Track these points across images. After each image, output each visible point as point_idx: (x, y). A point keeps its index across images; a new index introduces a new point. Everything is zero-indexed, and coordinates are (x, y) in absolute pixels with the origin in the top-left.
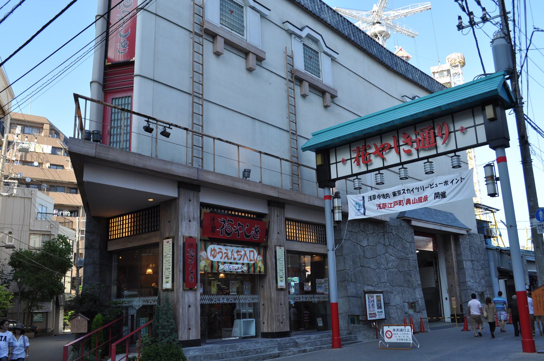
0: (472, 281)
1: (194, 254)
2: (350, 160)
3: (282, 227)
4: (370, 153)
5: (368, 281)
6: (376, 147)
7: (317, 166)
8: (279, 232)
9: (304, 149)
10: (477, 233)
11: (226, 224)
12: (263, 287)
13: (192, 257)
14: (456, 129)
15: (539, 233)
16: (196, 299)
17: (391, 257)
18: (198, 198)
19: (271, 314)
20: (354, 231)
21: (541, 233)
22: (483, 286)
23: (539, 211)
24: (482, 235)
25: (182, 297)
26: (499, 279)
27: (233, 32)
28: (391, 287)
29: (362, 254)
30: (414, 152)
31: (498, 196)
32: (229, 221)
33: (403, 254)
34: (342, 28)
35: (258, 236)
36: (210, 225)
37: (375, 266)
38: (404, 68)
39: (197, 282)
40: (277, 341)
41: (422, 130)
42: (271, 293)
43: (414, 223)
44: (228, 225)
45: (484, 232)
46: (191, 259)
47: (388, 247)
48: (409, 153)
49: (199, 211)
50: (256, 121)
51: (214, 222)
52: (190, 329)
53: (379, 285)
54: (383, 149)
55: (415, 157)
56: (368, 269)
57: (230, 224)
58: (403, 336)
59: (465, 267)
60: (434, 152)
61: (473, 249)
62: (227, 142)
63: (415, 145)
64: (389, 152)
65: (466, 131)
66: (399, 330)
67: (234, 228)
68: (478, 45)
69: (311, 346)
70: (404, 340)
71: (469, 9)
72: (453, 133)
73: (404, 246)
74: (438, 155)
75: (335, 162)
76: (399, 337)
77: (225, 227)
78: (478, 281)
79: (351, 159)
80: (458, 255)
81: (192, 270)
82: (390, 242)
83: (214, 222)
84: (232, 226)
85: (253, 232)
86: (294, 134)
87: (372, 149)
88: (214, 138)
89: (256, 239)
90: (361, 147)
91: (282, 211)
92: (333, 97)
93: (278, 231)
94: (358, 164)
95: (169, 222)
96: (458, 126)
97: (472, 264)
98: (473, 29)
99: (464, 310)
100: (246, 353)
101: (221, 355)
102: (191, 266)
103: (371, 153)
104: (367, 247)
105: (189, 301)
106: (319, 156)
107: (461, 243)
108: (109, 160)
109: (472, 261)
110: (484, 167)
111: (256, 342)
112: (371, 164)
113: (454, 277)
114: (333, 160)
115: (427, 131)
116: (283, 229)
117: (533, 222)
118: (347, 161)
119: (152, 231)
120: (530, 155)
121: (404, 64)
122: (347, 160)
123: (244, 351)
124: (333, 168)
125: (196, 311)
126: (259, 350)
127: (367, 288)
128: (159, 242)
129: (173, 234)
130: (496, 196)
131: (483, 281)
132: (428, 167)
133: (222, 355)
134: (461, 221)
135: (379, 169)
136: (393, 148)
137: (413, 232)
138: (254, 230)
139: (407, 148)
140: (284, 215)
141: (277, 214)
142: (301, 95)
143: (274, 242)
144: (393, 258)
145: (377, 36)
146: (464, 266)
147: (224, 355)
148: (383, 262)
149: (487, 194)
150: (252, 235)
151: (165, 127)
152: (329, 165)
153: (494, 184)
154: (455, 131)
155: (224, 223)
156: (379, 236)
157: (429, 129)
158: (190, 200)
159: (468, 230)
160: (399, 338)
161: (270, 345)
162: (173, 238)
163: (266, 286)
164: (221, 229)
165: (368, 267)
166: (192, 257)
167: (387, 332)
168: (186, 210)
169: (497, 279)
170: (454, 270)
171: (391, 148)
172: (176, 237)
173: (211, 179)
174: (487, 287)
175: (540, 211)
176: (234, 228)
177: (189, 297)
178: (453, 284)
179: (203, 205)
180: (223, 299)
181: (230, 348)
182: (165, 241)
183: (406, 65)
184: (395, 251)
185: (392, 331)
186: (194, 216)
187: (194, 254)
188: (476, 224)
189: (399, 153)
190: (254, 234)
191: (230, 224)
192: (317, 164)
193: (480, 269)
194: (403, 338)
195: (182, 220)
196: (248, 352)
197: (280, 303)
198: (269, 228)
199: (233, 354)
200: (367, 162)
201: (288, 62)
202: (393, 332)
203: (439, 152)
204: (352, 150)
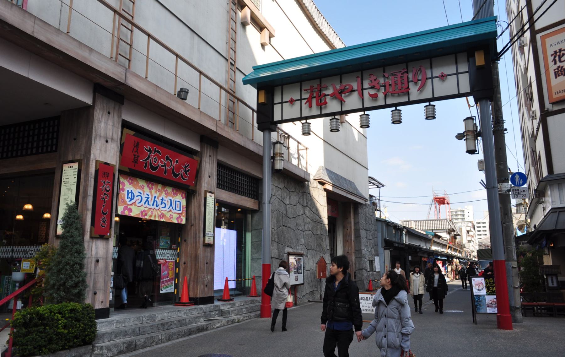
0: (365, 250)
3: (214, 170)
4: (327, 94)
5: (288, 242)
6: (335, 88)
7: (258, 104)
8: (210, 175)
11: (152, 155)
12: (185, 241)
13: (106, 192)
14: (434, 76)
17: (308, 219)
19: (195, 275)
20: (279, 187)
22: (372, 255)
25: (88, 246)
26: (385, 249)
28: (306, 250)
29: (284, 212)
30: (381, 95)
31: (478, 153)
35: (187, 177)
36: (132, 152)
37: (294, 226)
39: (111, 227)
40: (201, 309)
41: (393, 74)
42: (196, 249)
44: (154, 156)
46: (105, 194)
47: (306, 208)
48: (374, 97)
50: (195, 35)
51: (137, 149)
52: (95, 294)
53: (297, 248)
54: (342, 92)
55: (381, 102)
57: (156, 155)
59: (361, 236)
60: (405, 99)
63: (383, 90)
64: (348, 96)
65: (446, 79)
66: (364, 298)
69: (237, 315)
70: (369, 310)
72: (431, 80)
75: (280, 101)
77: (150, 159)
78: (369, 250)
79: (301, 100)
80: (356, 224)
81: (105, 209)
82: (308, 203)
83: (137, 149)
85: (182, 171)
87: (330, 90)
89: (185, 180)
90: (316, 86)
91: (215, 151)
92: (271, 36)
93: (209, 174)
94: (310, 106)
96: (437, 72)
97: (366, 233)
99: (357, 277)
100: (168, 327)
101: (137, 330)
102: (104, 204)
103: (328, 95)
104: (289, 206)
105: (97, 253)
107: (359, 212)
109: (366, 230)
110: (464, 120)
111: (178, 311)
112: (326, 107)
113: (351, 244)
114: (277, 99)
115: (399, 75)
116: (214, 172)
117: (502, 187)
118: (296, 102)
119: (42, 152)
123: (167, 323)
124: (277, 109)
126: (184, 322)
128: (55, 168)
129: (81, 157)
130: (476, 153)
131: (373, 249)
132: (396, 116)
133: (139, 330)
135: (333, 114)
136: (355, 91)
138: (183, 169)
139: (372, 92)
140: (216, 157)
141: (210, 153)
142: (241, 23)
143: (204, 187)
144: (309, 220)
146: (360, 235)
147: (141, 330)
148: (301, 223)
149: (466, 150)
150: (180, 174)
152: (273, 104)
154: (432, 78)
155: (150, 153)
156: (299, 196)
157: (402, 73)
158: (109, 113)
161: (195, 313)
162: (80, 162)
163: (190, 240)
164: (145, 160)
165: (289, 227)
166: (106, 192)
168: (103, 125)
170: (351, 238)
171: (352, 91)
172: (84, 162)
175: (517, 174)
177: (97, 248)
178: (350, 252)
179: (125, 125)
182: (66, 167)
186: (112, 135)
189: (362, 95)
192: (259, 102)
193: (371, 238)
194: (368, 309)
195: (95, 138)
196: (172, 325)
197: (206, 262)
198: (199, 169)
199: (153, 329)
200: (321, 104)
203: (411, 100)
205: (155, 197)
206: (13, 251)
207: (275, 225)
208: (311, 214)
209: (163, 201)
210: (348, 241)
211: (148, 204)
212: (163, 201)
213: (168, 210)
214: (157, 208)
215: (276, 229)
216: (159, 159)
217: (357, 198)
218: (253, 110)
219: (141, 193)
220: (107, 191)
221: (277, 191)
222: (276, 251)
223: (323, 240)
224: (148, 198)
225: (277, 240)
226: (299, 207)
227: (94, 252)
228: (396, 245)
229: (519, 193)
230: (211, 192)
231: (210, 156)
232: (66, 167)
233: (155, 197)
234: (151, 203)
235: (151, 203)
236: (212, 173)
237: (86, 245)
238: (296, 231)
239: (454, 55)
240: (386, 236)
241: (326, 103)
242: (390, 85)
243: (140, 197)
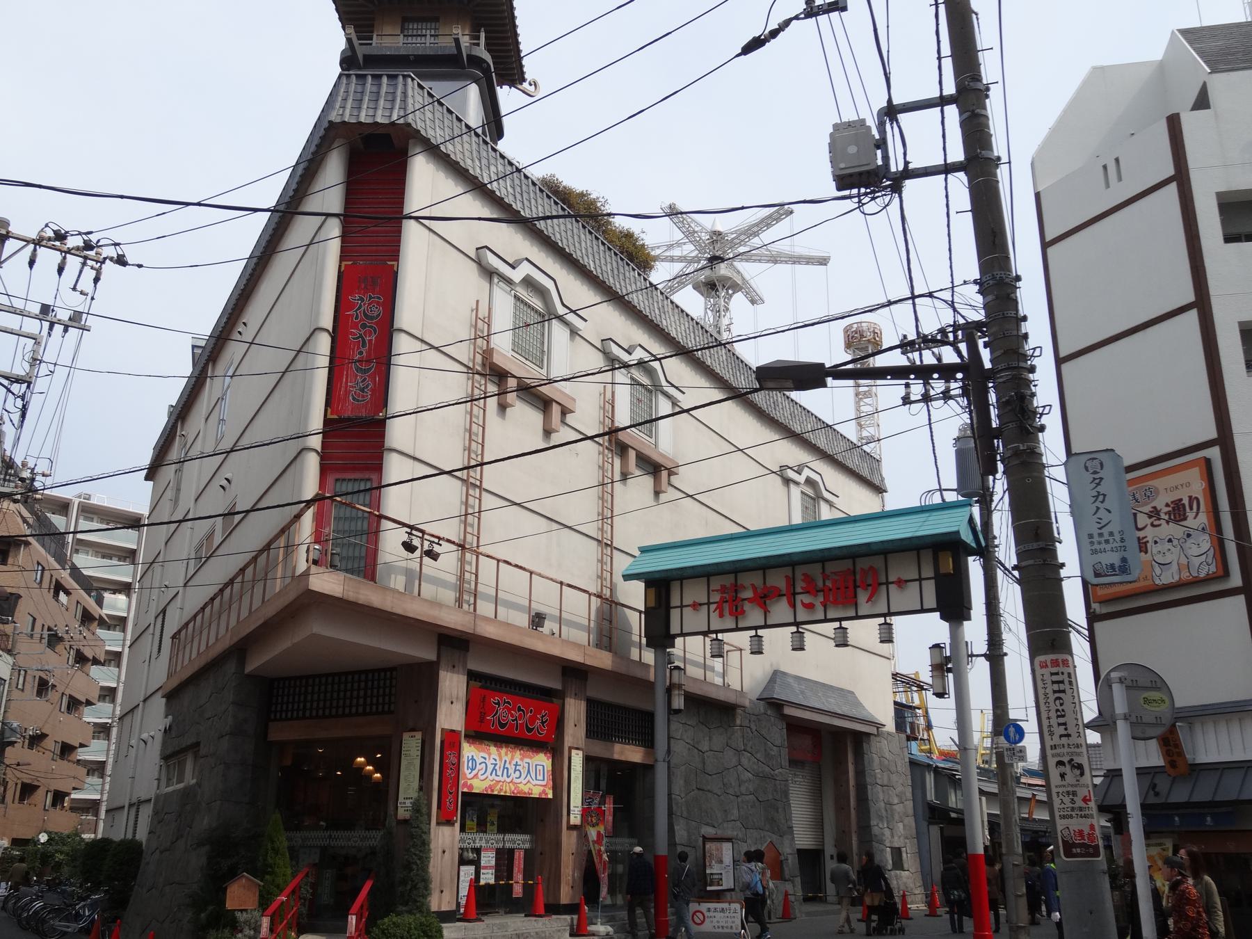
1: (455, 761)
2: (706, 606)
9: (627, 577)
10: (894, 731)
12: (542, 821)
15: (1007, 761)
16: (453, 840)
18: (465, 664)
21: (1010, 762)
22: (900, 837)
23: (1009, 726)
24: (903, 736)
26: (930, 823)
27: (527, 362)
32: (505, 702)
33: (767, 769)
34: (693, 342)
35: (544, 730)
38: (789, 412)
43: (788, 711)
45: (906, 728)
47: (743, 755)
49: (465, 685)
52: (442, 892)
56: (710, 795)
57: (506, 707)
58: (724, 920)
61: (886, 762)
62: (516, 566)
67: (512, 716)
68: (940, 474)
71: (923, 358)
73: (769, 754)
74: (857, 617)
76: (718, 922)
81: (451, 788)
84: (509, 710)
86: (606, 545)
88: (498, 561)
94: (721, 616)
95: (416, 702)
98: (928, 406)
103: (745, 599)
106: (652, 591)
107: (865, 752)
108: (360, 602)
114: (675, 601)
120: (1002, 633)
121: (789, 404)
122: (701, 605)
124: (675, 615)
125: (453, 859)
127: (708, 831)
134: (866, 707)
136: (784, 595)
137: (785, 726)
139: (807, 599)
145: (716, 286)
151: (432, 542)
152: (668, 608)
153: (943, 677)
154: (887, 583)
158: (454, 667)
159: (879, 726)
160: (716, 925)
165: (709, 791)
167: (695, 913)
168: (447, 683)
169: (925, 824)
173: (490, 631)
174: (906, 838)
176: (512, 716)
177: (443, 835)
180: (481, 839)
181: (499, 929)
182: (406, 736)
183: (791, 404)
184: (754, 763)
185: (704, 911)
187: (455, 761)
188: (893, 714)
189: (793, 606)
190: (540, 728)
191: (506, 707)
195: (441, 701)
200: (737, 613)
201: (606, 414)
202: (707, 914)
204: (711, 588)
205: (506, 761)
206: (330, 837)
207: (683, 789)
208: (754, 763)
209: (518, 768)
210: (843, 809)
211: (496, 775)
212: (518, 768)
213: (525, 782)
214: (509, 780)
215: (683, 795)
216: (510, 712)
217: (857, 724)
218: (640, 612)
219: (485, 758)
220: (453, 765)
221: (686, 731)
222: (685, 834)
223: (780, 810)
224: (496, 765)
225: (685, 814)
226: (729, 753)
227: (440, 841)
228: (953, 815)
229: (1014, 754)
230: (577, 749)
231: (576, 695)
232: (406, 736)
233: (506, 761)
234: (499, 773)
235: (499, 773)
236: (579, 720)
237: (432, 830)
238: (722, 797)
239: (915, 552)
240: (931, 796)
241: (743, 612)
242: (830, 590)
243: (484, 765)
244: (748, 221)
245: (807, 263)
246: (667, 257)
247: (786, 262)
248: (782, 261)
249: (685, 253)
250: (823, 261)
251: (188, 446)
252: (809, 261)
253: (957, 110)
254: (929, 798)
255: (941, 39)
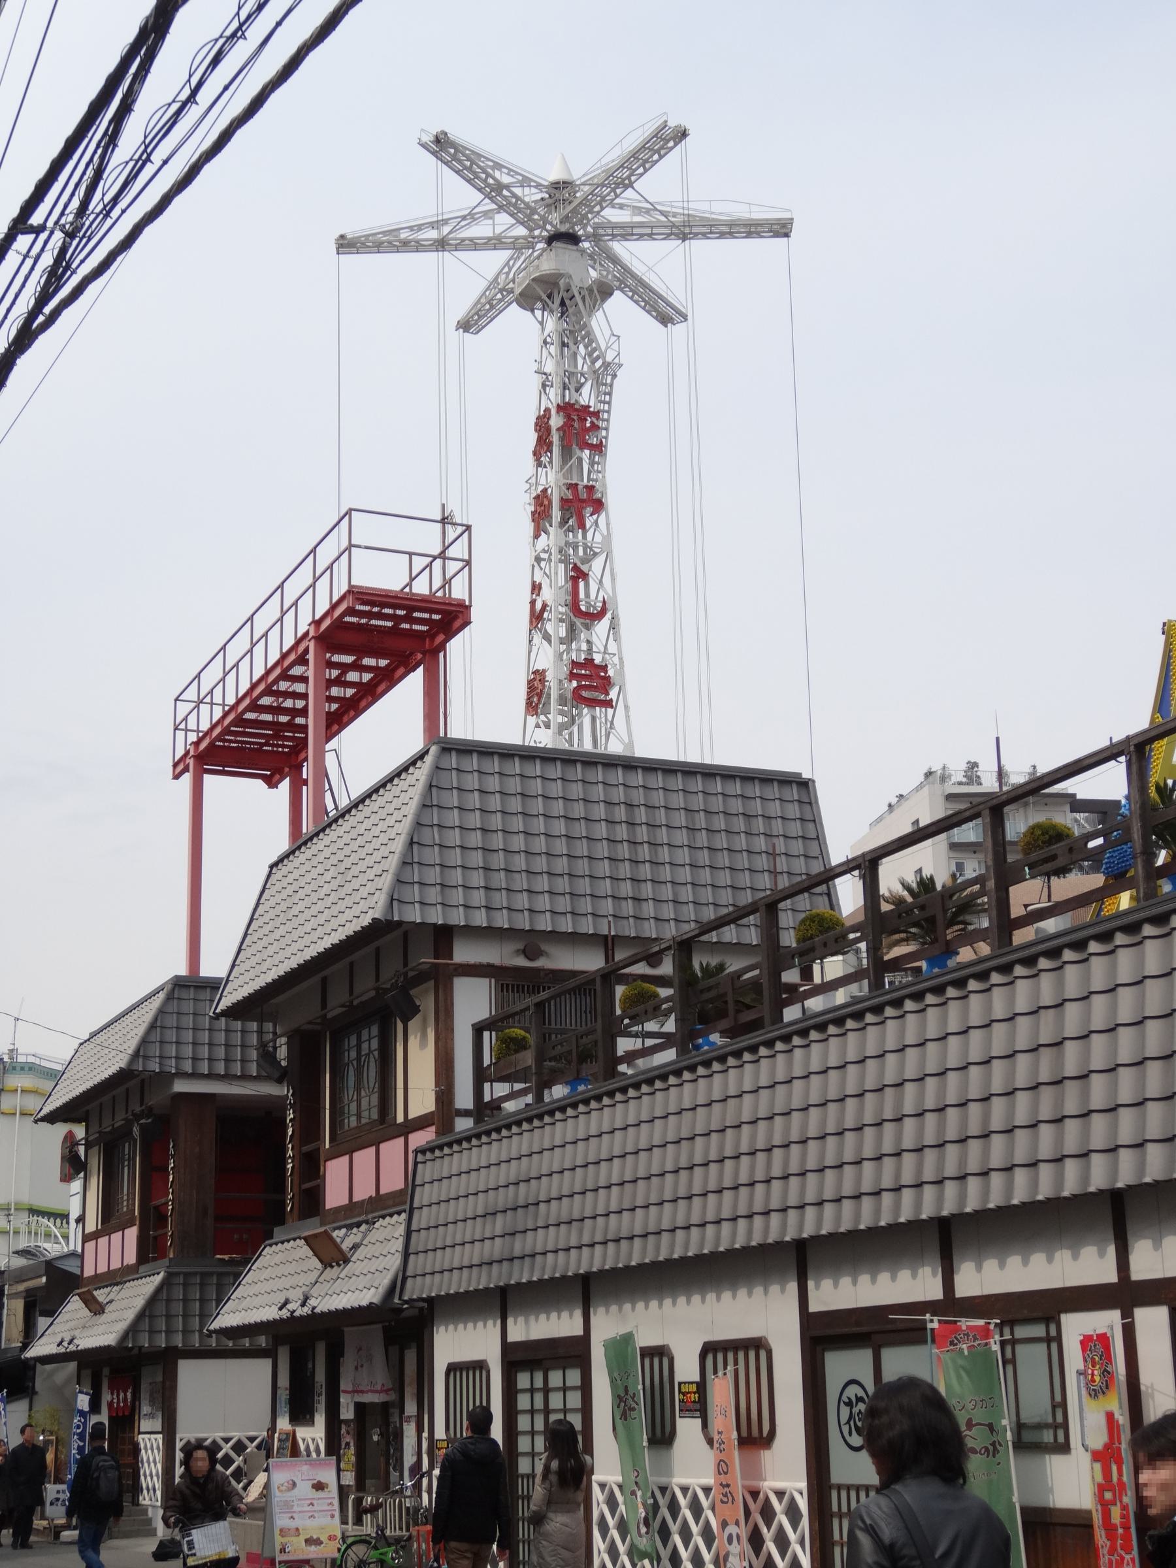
136: (985, 911)
244: (604, 161)
245: (749, 235)
246: (463, 240)
247: (705, 236)
248: (696, 234)
249: (498, 230)
250: (782, 229)
251: (611, 636)
252: (752, 229)
253: (18, 361)
254: (674, 1057)
255: (27, 285)
